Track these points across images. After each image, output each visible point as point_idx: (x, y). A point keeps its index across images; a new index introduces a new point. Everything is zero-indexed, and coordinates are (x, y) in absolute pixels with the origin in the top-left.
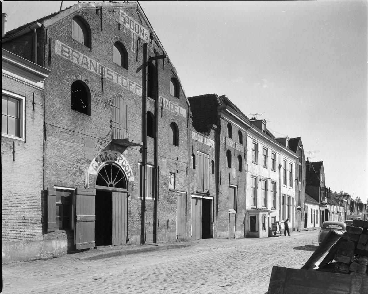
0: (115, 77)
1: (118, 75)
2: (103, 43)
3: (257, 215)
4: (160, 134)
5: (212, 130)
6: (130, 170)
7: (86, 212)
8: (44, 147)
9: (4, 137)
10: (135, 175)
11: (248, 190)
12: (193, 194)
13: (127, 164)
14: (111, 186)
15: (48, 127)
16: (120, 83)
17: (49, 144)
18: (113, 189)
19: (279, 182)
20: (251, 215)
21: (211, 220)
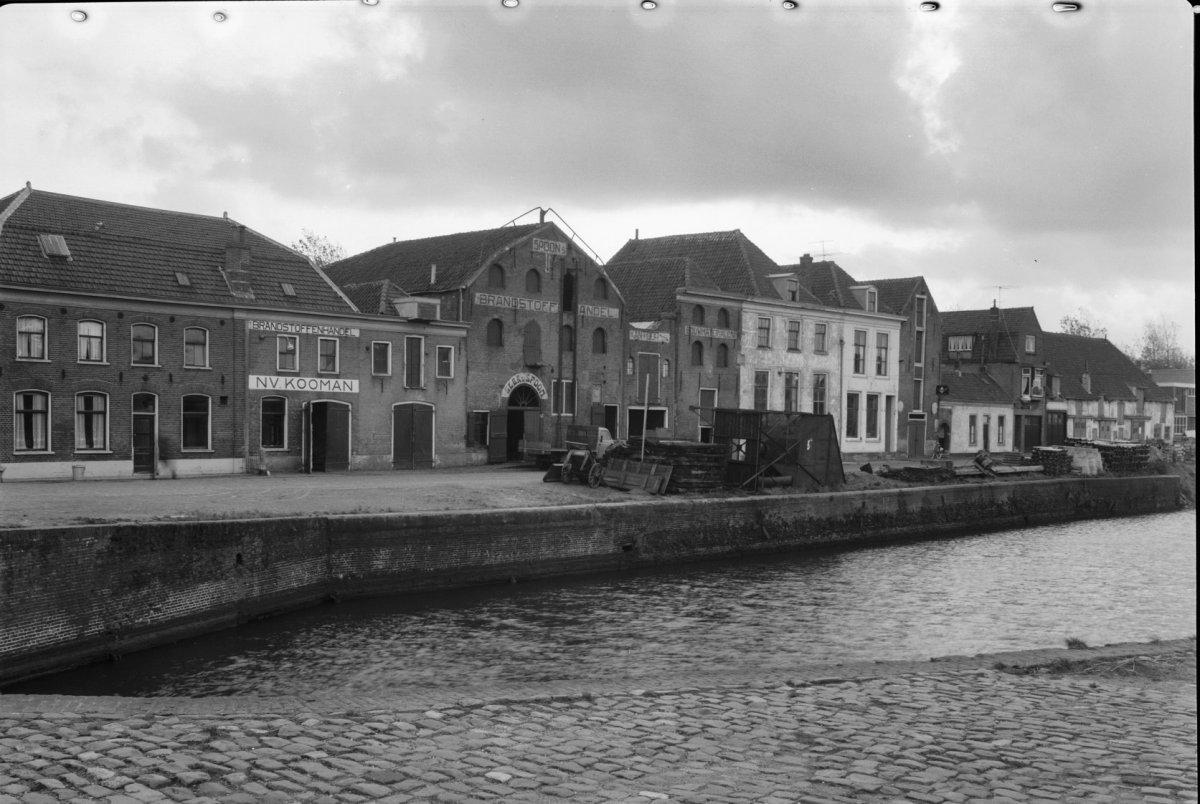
0: (527, 303)
1: (530, 302)
2: (517, 276)
3: (858, 439)
4: (93, 724)
5: (631, 338)
6: (543, 388)
7: (496, 431)
8: (466, 381)
9: (1187, 744)
10: (549, 392)
11: (744, 392)
12: (630, 405)
13: (540, 382)
14: (523, 405)
15: (470, 365)
16: (533, 308)
17: (470, 378)
18: (523, 408)
19: (845, 373)
20: (854, 439)
21: (919, 484)
